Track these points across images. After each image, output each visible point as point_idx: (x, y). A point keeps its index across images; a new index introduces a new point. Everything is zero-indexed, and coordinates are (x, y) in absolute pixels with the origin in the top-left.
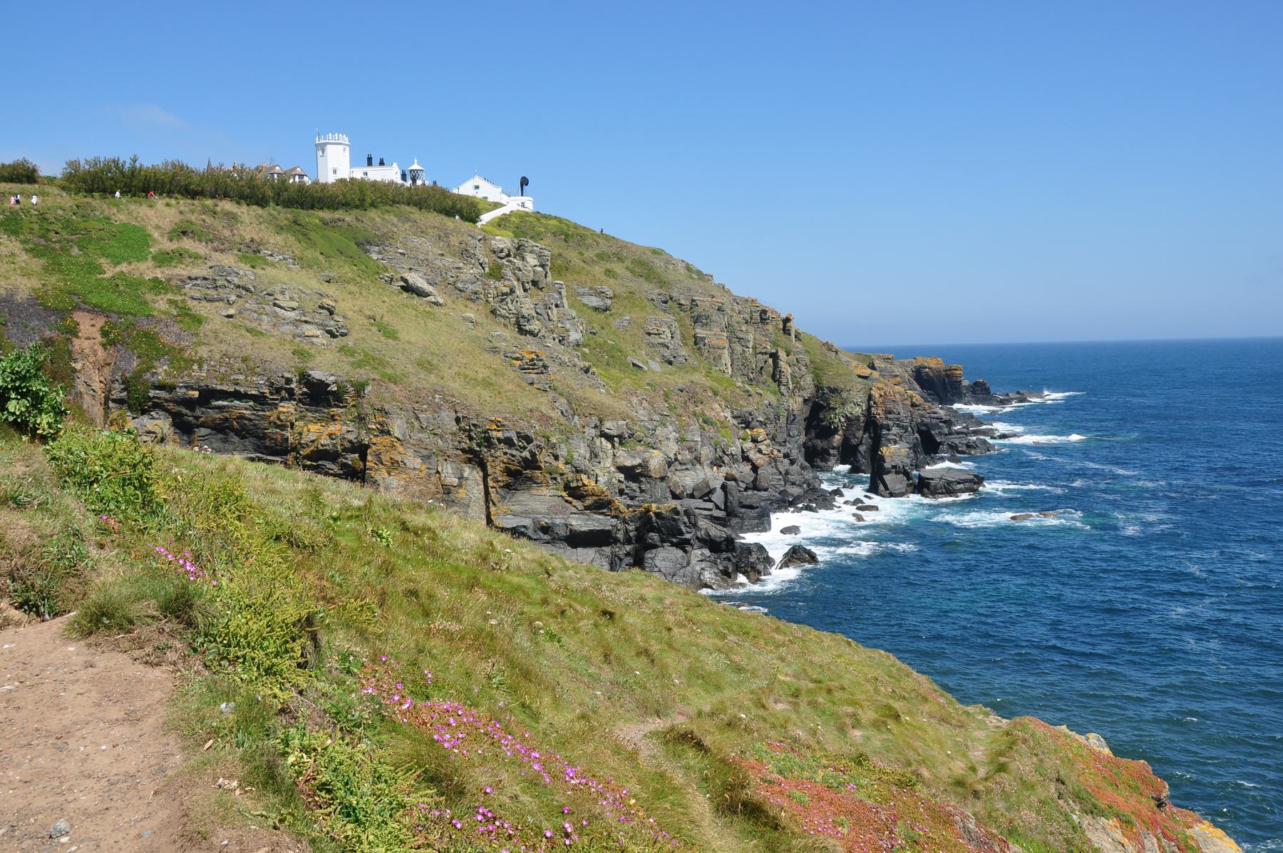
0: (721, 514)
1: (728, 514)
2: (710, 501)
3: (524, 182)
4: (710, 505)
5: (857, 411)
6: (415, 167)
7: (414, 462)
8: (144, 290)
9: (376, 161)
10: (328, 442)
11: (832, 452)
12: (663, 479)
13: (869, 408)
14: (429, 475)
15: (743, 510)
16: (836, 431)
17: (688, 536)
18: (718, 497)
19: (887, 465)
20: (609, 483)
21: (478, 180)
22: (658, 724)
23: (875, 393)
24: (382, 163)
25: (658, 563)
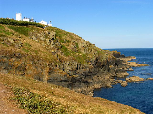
6: (32, 19)
7: (34, 68)
24: (27, 18)
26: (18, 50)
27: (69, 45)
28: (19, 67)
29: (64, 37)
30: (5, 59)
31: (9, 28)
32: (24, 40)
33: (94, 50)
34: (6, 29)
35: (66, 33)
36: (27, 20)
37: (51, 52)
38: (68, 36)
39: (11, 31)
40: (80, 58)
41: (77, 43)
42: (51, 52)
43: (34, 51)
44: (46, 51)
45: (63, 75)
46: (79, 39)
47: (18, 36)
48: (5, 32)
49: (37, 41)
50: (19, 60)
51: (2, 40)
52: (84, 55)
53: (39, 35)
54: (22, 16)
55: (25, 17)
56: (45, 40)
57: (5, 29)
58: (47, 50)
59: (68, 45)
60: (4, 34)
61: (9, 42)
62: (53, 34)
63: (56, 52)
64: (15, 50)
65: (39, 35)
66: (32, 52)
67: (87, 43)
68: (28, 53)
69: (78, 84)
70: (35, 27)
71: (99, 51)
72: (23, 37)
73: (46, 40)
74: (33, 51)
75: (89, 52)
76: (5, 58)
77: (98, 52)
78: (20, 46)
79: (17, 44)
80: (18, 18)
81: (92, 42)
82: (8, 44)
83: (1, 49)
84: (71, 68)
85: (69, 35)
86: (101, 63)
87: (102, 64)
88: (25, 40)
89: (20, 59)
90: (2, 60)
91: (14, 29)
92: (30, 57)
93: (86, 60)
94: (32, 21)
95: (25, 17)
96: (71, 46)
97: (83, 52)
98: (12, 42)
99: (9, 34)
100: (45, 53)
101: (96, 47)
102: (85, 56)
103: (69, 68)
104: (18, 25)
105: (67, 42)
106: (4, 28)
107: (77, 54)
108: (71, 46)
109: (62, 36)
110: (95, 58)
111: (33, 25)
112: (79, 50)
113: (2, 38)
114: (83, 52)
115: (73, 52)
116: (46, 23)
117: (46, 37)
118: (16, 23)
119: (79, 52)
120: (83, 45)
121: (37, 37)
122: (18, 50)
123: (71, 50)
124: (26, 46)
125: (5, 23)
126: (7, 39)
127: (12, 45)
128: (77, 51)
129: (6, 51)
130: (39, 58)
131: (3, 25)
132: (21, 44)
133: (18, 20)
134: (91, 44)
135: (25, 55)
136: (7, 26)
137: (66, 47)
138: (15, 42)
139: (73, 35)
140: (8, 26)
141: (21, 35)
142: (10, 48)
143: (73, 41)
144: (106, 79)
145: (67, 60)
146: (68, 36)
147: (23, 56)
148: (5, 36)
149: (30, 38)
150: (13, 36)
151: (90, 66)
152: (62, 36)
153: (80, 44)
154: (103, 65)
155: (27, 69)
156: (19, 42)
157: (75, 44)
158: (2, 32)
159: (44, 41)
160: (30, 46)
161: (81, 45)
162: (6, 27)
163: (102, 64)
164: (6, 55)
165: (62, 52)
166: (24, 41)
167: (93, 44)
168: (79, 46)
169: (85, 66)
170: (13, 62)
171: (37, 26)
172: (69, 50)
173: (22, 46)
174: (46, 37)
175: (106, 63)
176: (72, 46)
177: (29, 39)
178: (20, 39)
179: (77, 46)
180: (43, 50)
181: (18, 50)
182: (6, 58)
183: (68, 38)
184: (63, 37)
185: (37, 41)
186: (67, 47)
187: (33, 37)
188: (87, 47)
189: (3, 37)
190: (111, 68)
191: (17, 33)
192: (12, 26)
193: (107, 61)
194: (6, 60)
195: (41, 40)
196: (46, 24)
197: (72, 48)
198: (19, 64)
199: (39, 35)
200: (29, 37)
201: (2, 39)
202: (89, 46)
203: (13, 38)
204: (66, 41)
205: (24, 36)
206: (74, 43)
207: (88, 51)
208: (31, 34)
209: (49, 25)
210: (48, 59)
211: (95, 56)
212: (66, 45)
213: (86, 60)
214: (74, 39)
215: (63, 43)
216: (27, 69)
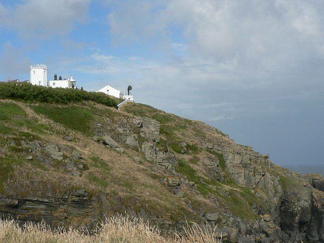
3: (130, 88)
13: (312, 202)
24: (60, 79)
26: (78, 180)
27: (198, 159)
29: (181, 136)
31: (38, 110)
33: (272, 173)
34: (30, 115)
35: (185, 124)
36: (64, 84)
37: (164, 184)
38: (189, 132)
39: (43, 120)
40: (236, 201)
41: (220, 152)
42: (166, 183)
43: (122, 183)
44: (151, 181)
47: (65, 136)
48: (30, 123)
49: (118, 149)
50: (82, 211)
51: (27, 150)
52: (246, 193)
54: (49, 71)
55: (56, 76)
56: (141, 147)
57: (26, 115)
58: (154, 177)
59: (195, 161)
60: (30, 131)
61: (48, 155)
63: (179, 185)
64: (68, 182)
65: (121, 132)
66: (116, 186)
67: (249, 152)
68: (108, 191)
70: (99, 106)
72: (79, 139)
73: (143, 147)
74: (116, 181)
75: (257, 180)
77: (283, 182)
78: (81, 166)
79: (71, 160)
80: (38, 77)
82: (43, 161)
83: (28, 179)
84: (226, 234)
85: (195, 129)
86: (293, 215)
87: (297, 218)
88: (87, 149)
89: (84, 208)
90: (31, 212)
91: (50, 114)
92: (116, 202)
93: (254, 206)
95: (56, 76)
96: (202, 165)
97: (242, 181)
98: (57, 155)
99: (41, 132)
100: (152, 187)
102: (249, 193)
104: (57, 102)
105: (191, 152)
106: (24, 111)
107: (227, 187)
108: (202, 165)
109: (176, 132)
110: (276, 200)
111: (93, 100)
112: (228, 174)
113: (27, 144)
114: (242, 181)
115: (213, 183)
116: (119, 92)
117: (141, 140)
118: (51, 96)
121: (117, 137)
122: (76, 181)
123: (206, 175)
124: (96, 166)
125: (21, 97)
126: (41, 146)
127: (58, 164)
128: (223, 178)
129: (44, 184)
130: (139, 205)
131: (20, 104)
132: (82, 161)
135: (99, 200)
136: (30, 106)
137: (191, 165)
138: (65, 157)
139: (204, 127)
140: (32, 105)
141: (73, 133)
142: (53, 175)
143: (207, 147)
145: (212, 211)
146: (189, 132)
147: (94, 198)
148: (35, 138)
150: (53, 136)
151: (269, 227)
152: (176, 132)
154: (302, 224)
157: (214, 156)
158: (22, 124)
159: (138, 151)
160: (104, 164)
161: (232, 160)
162: (28, 110)
163: (297, 218)
164: (43, 196)
165: (192, 183)
166: (86, 152)
167: (264, 155)
168: (228, 162)
169: (256, 226)
171: (103, 103)
172: (200, 174)
173: (84, 166)
174: (141, 140)
175: (309, 216)
176: (207, 162)
177: (96, 144)
179: (222, 164)
180: (142, 178)
181: (76, 181)
183: (192, 140)
184: (178, 134)
185: (118, 149)
186: (195, 167)
187: (107, 138)
188: (250, 164)
189: (30, 141)
191: (60, 127)
192: (42, 105)
193: (314, 210)
194: (43, 212)
195: (127, 147)
196: (118, 96)
197: (210, 169)
199: (121, 130)
200: (96, 138)
201: (27, 146)
203: (56, 142)
204: (188, 146)
205: (79, 135)
206: (210, 152)
207: (252, 178)
208: (97, 130)
210: (165, 207)
211: (276, 192)
212: (191, 161)
213: (254, 206)
214: (210, 141)
215: (180, 152)
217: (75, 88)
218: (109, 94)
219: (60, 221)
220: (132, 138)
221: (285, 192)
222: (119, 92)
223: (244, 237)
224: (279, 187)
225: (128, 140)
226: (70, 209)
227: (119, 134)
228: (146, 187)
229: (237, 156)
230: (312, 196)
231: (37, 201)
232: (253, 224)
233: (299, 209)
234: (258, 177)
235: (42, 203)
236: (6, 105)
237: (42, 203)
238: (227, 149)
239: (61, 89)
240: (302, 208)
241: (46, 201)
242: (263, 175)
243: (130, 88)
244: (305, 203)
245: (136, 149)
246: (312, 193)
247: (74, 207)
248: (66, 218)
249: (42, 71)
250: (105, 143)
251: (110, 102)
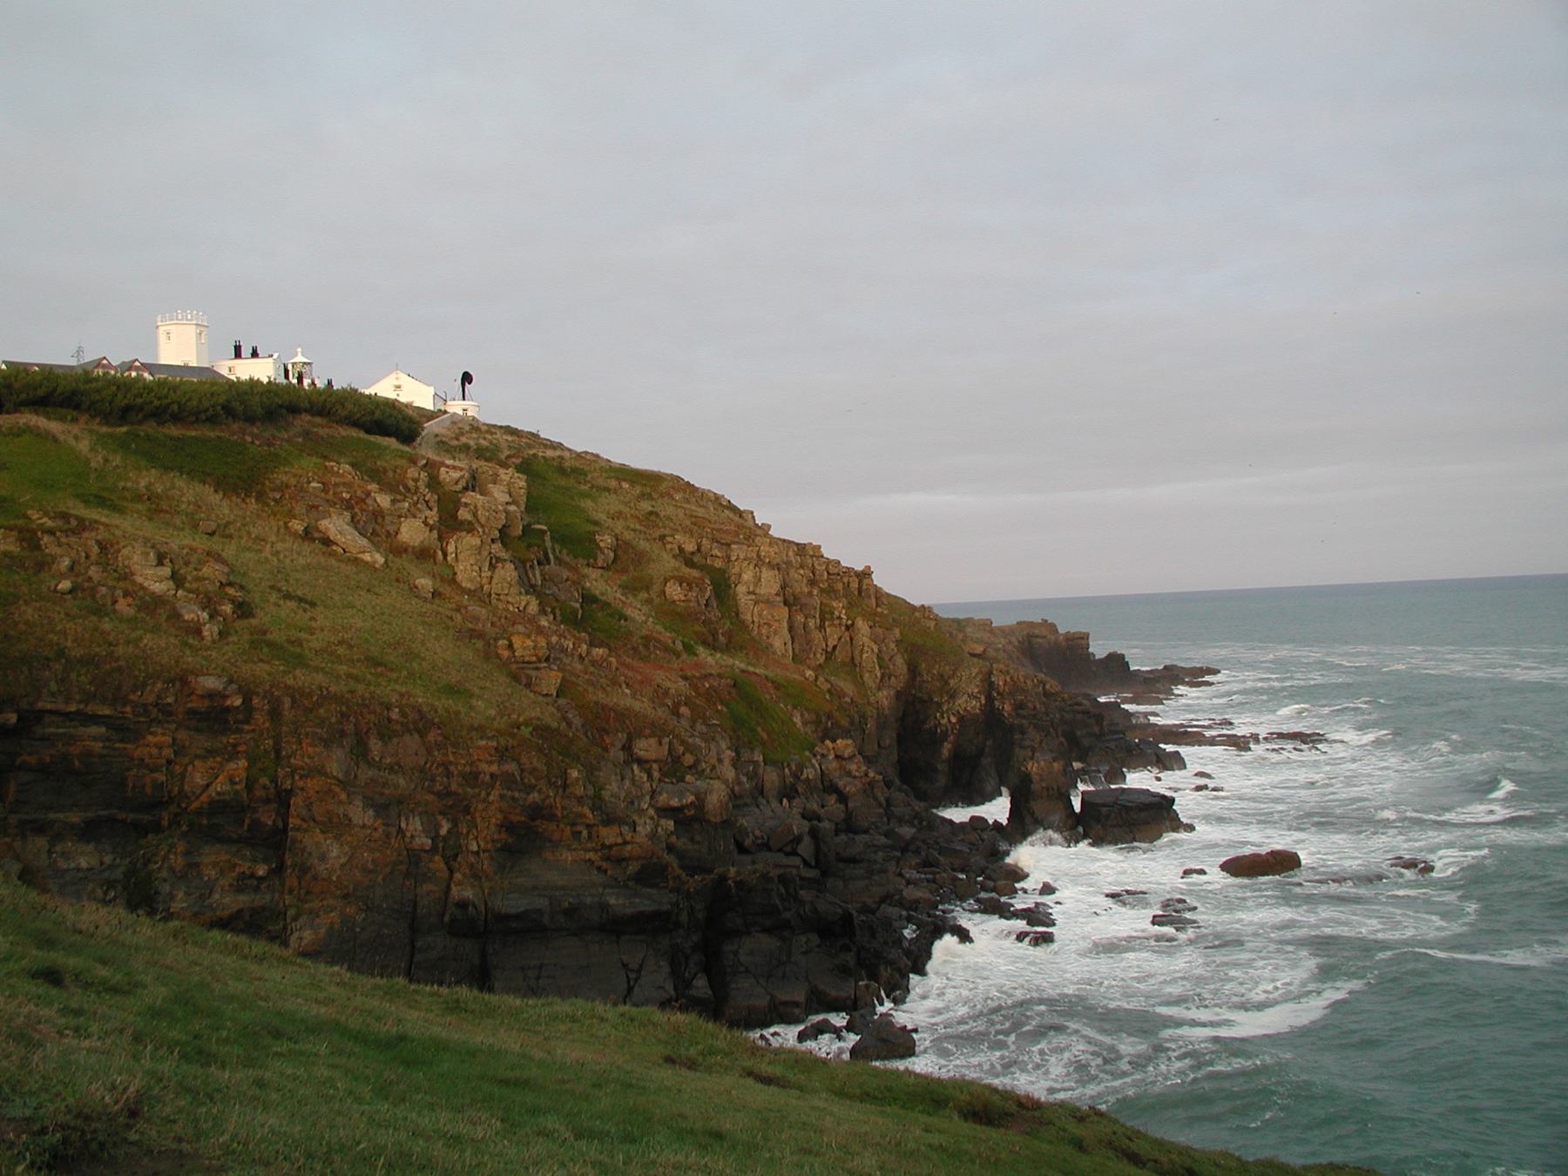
0: (812, 873)
1: (824, 873)
2: (794, 853)
3: (467, 378)
4: (796, 861)
5: (974, 706)
6: (300, 359)
7: (360, 815)
8: (675, 591)
9: (246, 351)
10: (227, 788)
11: (940, 767)
12: (726, 823)
13: (990, 699)
14: (388, 835)
15: (841, 865)
16: (945, 735)
17: (787, 915)
18: (806, 848)
19: (1035, 787)
20: (653, 836)
21: (404, 379)
22: (253, 621)
23: (998, 680)
24: (255, 354)
25: (743, 958)
28: (219, 807)
30: (95, 739)
32: (261, 546)
33: (872, 617)
36: (261, 370)
45: (633, 868)
46: (731, 526)
53: (384, 500)
62: (502, 494)
69: (768, 942)
71: (922, 637)
73: (451, 548)
75: (831, 643)
76: (95, 730)
78: (228, 608)
81: (846, 552)
84: (691, 798)
86: (936, 740)
94: (300, 378)
101: (879, 594)
103: (675, 802)
110: (885, 698)
117: (449, 523)
119: (737, 638)
120: (770, 583)
121: (374, 526)
132: (231, 591)
133: (73, 362)
134: (836, 572)
143: (681, 549)
144: (474, 702)
149: (308, 535)
151: (849, 774)
153: (745, 577)
155: (298, 822)
156: (213, 572)
161: (754, 587)
162: (77, 437)
167: (859, 568)
168: (741, 589)
169: (809, 773)
170: (169, 762)
174: (449, 523)
178: (216, 544)
179: (722, 586)
182: (103, 729)
190: (1035, 778)
194: (97, 746)
195: (400, 550)
198: (220, 786)
199: (384, 500)
202: (829, 591)
207: (817, 636)
209: (456, 407)
216: (298, 822)
217: (306, 382)
218: (403, 399)
219: (152, 771)
220: (418, 523)
221: (913, 670)
222: (431, 391)
223: (774, 804)
224: (900, 661)
225: (404, 529)
226: (182, 735)
227: (378, 514)
228: (288, 596)
229: (767, 574)
230: (991, 684)
231: (78, 712)
232: (801, 767)
233: (954, 720)
234: (833, 635)
235: (95, 719)
236: (17, 432)
237: (95, 719)
238: (737, 551)
239: (253, 384)
240: (961, 719)
241: (107, 712)
242: (848, 628)
243: (467, 378)
244: (968, 702)
245: (423, 554)
246: (990, 673)
247: (197, 730)
248: (169, 762)
249: (192, 331)
250: (327, 542)
251: (395, 423)
